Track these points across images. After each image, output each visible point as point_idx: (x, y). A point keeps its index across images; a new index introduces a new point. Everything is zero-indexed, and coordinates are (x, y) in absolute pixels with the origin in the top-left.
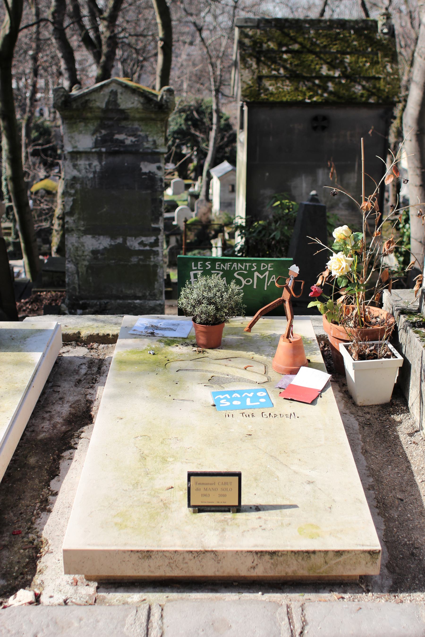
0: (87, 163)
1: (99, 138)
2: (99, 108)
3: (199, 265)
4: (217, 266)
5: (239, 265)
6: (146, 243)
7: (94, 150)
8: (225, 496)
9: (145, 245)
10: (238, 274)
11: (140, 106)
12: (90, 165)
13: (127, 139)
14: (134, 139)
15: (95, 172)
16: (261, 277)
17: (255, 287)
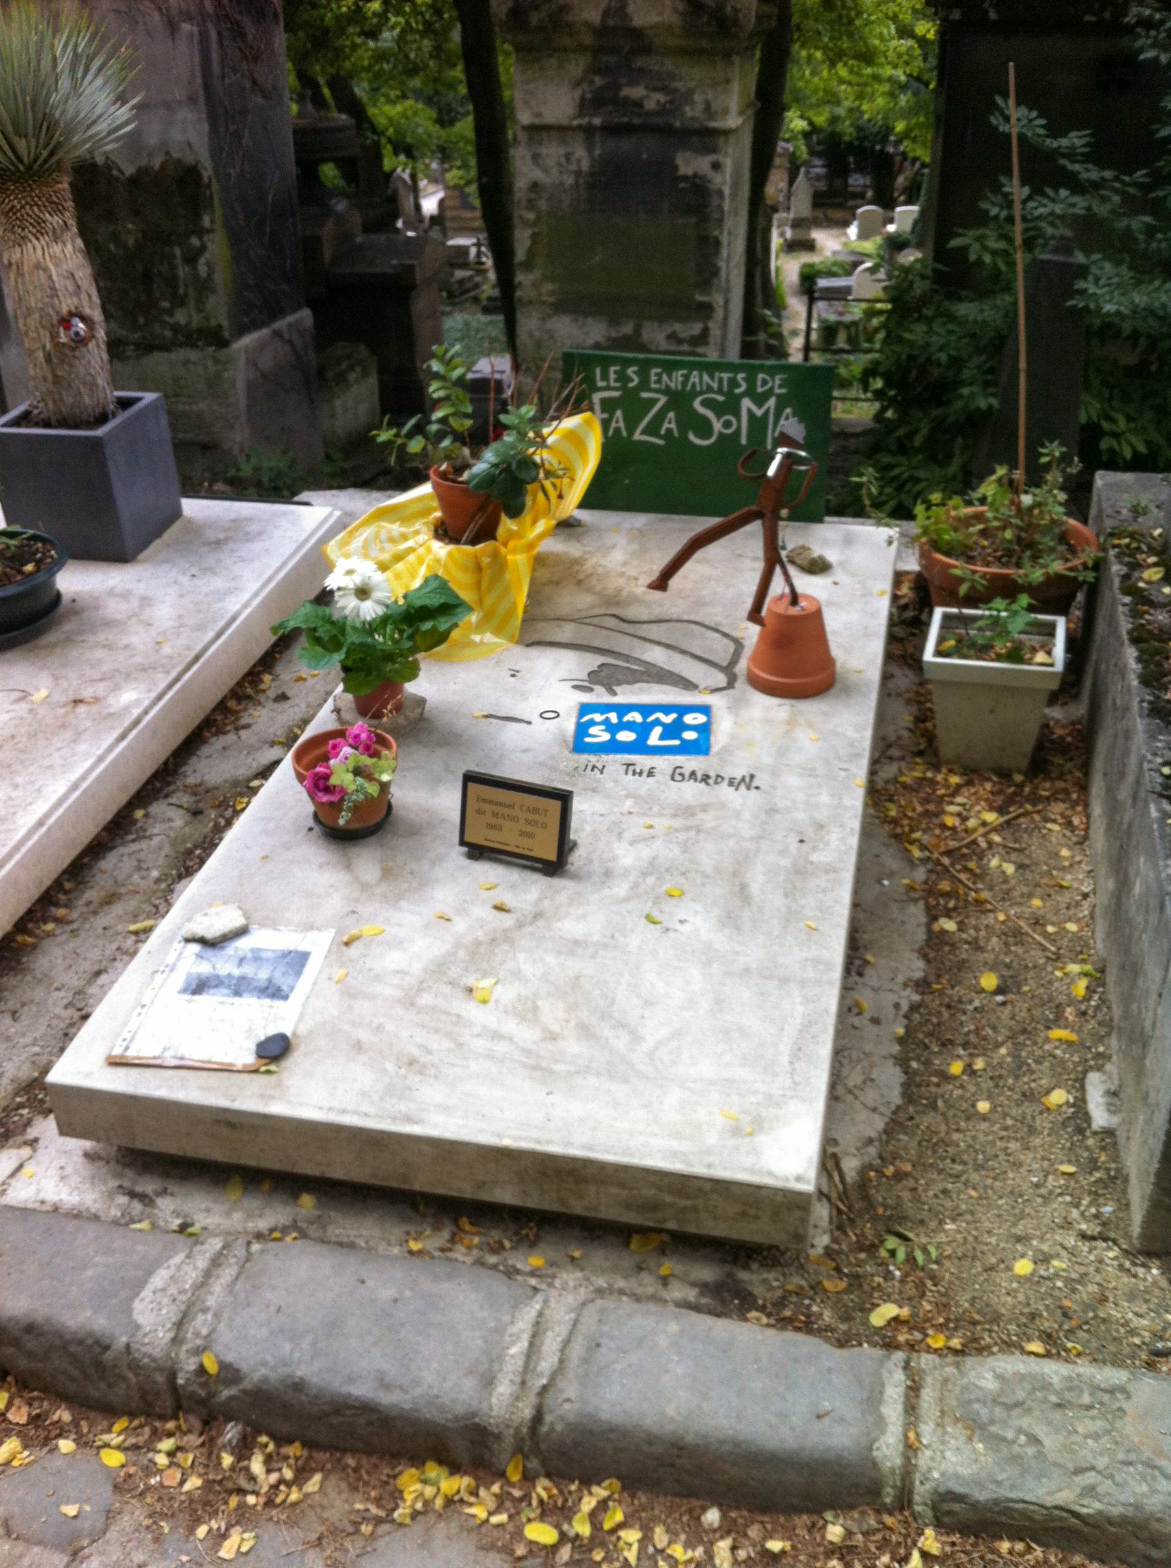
0: (562, 151)
1: (588, 96)
2: (587, 24)
3: (612, 376)
4: (653, 378)
5: (706, 378)
6: (683, 335)
7: (575, 123)
8: (531, 835)
9: (680, 341)
10: (704, 403)
11: (675, 19)
12: (568, 157)
13: (647, 97)
14: (662, 98)
15: (578, 173)
16: (759, 412)
17: (744, 441)
